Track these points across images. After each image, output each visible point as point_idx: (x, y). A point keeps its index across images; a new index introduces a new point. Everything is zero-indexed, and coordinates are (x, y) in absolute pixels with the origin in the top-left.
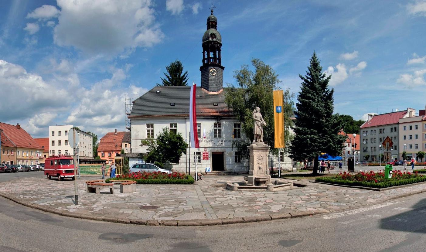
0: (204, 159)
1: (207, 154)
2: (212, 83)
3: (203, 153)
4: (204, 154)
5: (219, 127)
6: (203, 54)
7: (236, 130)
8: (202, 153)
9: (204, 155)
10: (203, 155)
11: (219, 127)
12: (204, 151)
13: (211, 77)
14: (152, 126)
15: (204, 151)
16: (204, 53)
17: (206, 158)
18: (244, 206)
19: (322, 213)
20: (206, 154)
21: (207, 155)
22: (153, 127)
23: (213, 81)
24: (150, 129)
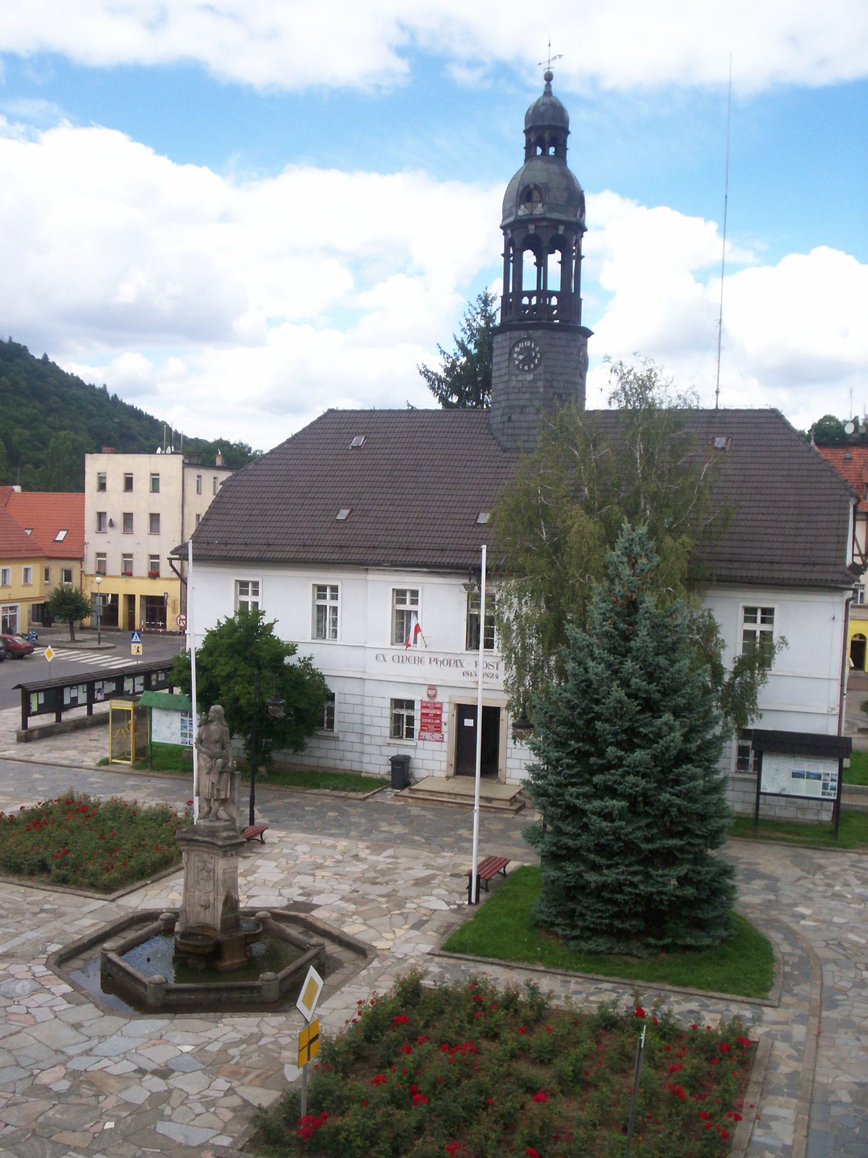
0: (424, 727)
1: (438, 712)
2: (522, 403)
3: (422, 707)
4: (425, 711)
5: (763, 621)
6: (583, 254)
7: (326, 606)
8: (417, 706)
9: (427, 714)
10: (422, 714)
11: (763, 621)
12: (427, 699)
13: (520, 378)
14: (768, 615)
15: (427, 699)
16: (512, 260)
17: (432, 727)
18: (676, 944)
19: (754, 1003)
20: (434, 711)
21: (435, 715)
22: (771, 621)
23: (527, 396)
24: (758, 627)
